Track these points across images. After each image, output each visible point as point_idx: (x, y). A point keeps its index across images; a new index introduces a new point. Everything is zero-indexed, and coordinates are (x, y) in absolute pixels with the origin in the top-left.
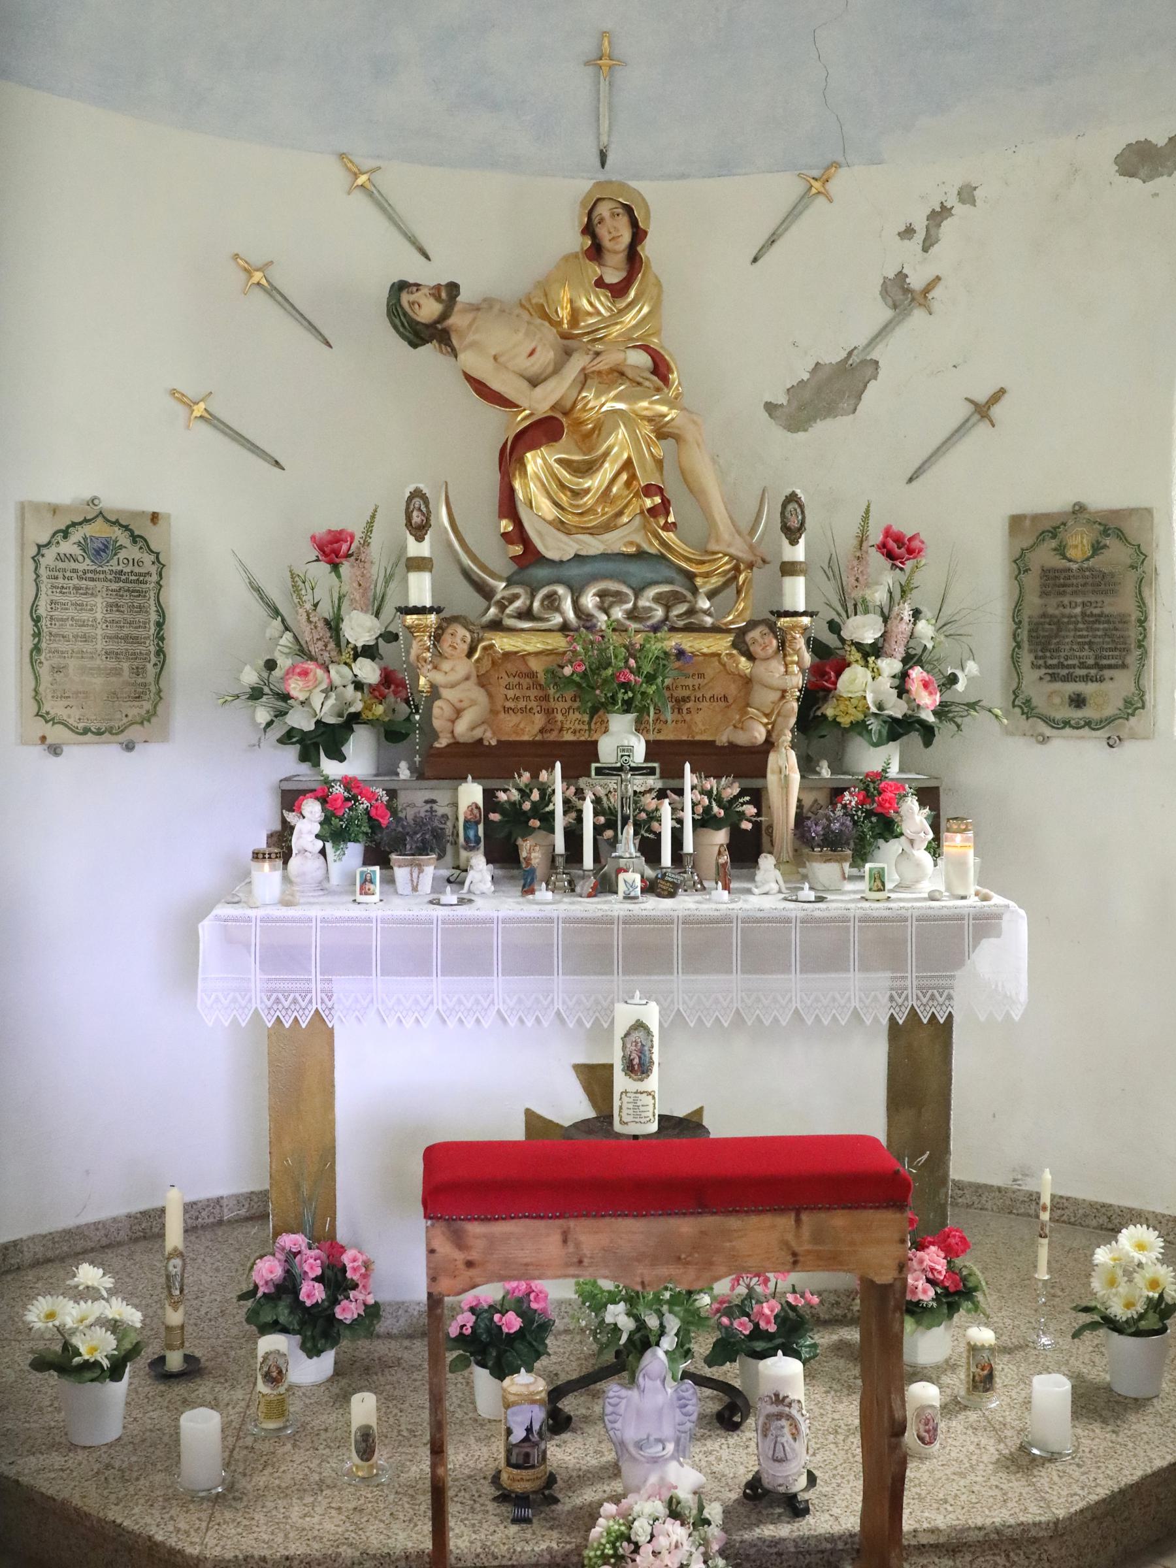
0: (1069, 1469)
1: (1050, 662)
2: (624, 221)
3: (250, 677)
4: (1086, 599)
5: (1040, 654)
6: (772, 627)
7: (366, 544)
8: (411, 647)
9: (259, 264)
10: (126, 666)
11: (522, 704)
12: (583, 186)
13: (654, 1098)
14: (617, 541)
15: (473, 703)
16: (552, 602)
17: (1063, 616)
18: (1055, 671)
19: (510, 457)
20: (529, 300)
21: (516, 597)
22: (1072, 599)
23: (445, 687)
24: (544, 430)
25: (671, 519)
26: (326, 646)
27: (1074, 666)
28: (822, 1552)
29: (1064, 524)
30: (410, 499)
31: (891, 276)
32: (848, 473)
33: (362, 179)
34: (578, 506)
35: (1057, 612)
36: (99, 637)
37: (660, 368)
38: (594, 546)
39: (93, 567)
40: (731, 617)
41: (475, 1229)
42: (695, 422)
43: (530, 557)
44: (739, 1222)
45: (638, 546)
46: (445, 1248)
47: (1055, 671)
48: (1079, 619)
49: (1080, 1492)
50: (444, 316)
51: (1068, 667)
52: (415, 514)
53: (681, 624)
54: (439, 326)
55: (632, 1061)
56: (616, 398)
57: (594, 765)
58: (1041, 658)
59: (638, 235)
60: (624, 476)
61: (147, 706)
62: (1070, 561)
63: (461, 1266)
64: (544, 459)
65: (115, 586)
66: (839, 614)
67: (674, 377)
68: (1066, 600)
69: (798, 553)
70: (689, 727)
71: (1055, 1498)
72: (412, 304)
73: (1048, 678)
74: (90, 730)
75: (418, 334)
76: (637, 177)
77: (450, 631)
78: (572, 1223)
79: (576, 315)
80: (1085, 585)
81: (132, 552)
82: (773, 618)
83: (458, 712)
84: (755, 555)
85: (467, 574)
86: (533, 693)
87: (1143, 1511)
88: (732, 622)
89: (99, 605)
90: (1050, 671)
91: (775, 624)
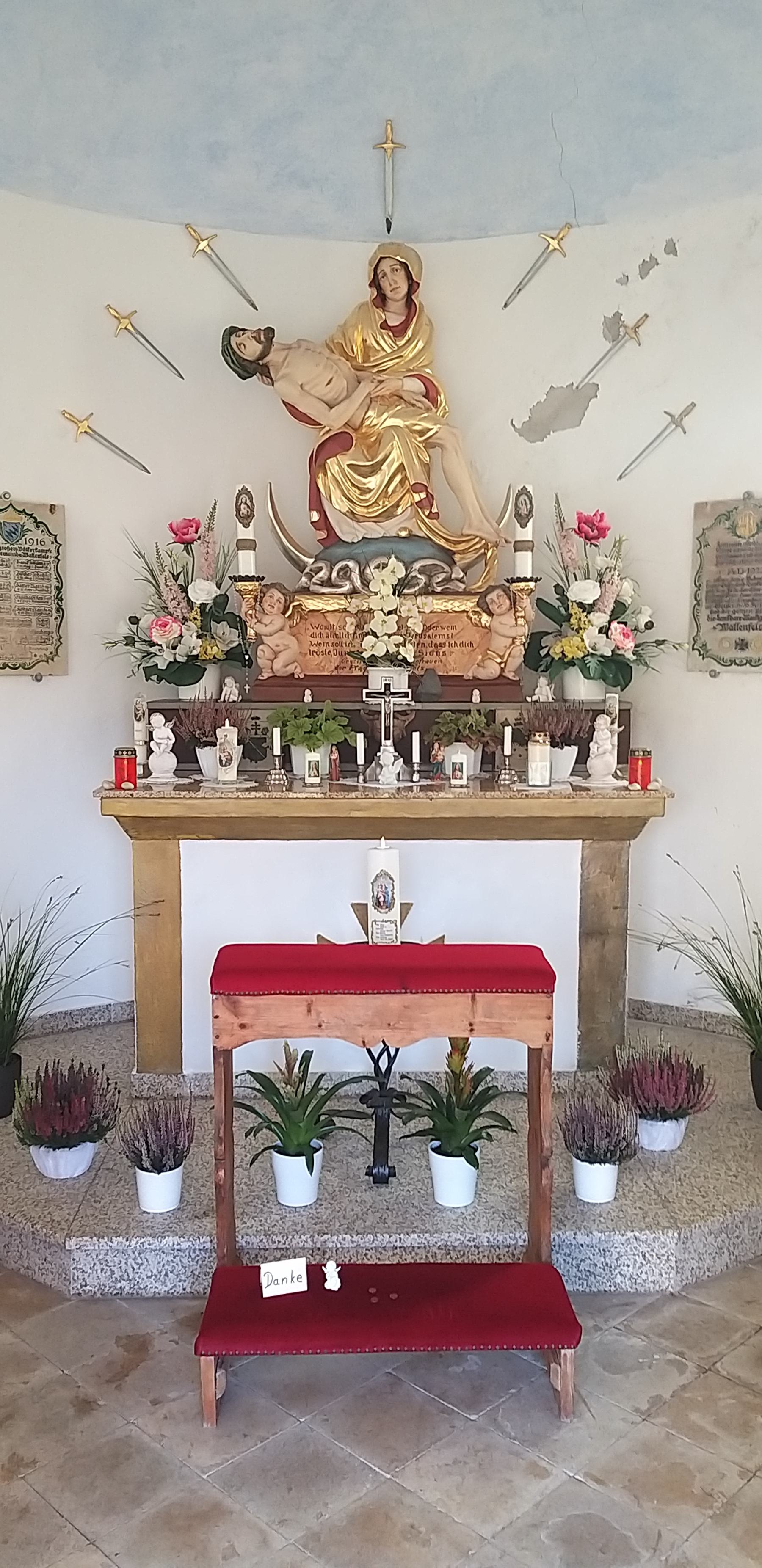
0: (696, 1199)
1: (721, 615)
2: (401, 276)
3: (124, 629)
4: (750, 567)
5: (714, 609)
6: (506, 591)
7: (210, 528)
8: (241, 607)
9: (125, 314)
10: (34, 619)
11: (322, 648)
12: (370, 249)
13: (396, 925)
14: (391, 527)
15: (287, 647)
16: (345, 573)
17: (733, 579)
18: (726, 622)
19: (317, 461)
20: (333, 342)
21: (321, 569)
22: (739, 567)
23: (266, 635)
24: (338, 442)
25: (434, 510)
26: (178, 604)
27: (740, 618)
28: (509, 1247)
29: (736, 509)
30: (238, 496)
31: (611, 316)
32: (573, 470)
33: (203, 245)
34: (367, 501)
35: (729, 577)
36: (13, 597)
37: (431, 393)
38: (376, 531)
39: (6, 546)
40: (480, 583)
41: (246, 1001)
42: (455, 435)
43: (331, 539)
44: (432, 1000)
45: (410, 531)
46: (226, 1016)
47: (726, 622)
48: (745, 582)
49: (702, 1214)
50: (264, 354)
51: (736, 619)
52: (243, 506)
53: (439, 589)
54: (261, 362)
55: (378, 899)
56: (393, 416)
57: (365, 691)
58: (715, 612)
59: (413, 286)
60: (398, 478)
61: (52, 648)
62: (740, 537)
63: (236, 1026)
64: (339, 465)
65: (24, 559)
66: (562, 580)
67: (441, 398)
68: (735, 568)
69: (526, 534)
70: (445, 665)
71: (681, 1218)
72: (238, 345)
73: (720, 627)
74: (8, 666)
75: (245, 369)
76: (417, 240)
77: (268, 594)
78: (314, 997)
79: (367, 349)
80: (751, 555)
81: (35, 534)
82: (508, 585)
83: (276, 654)
84: (499, 537)
85: (286, 551)
86: (331, 640)
87: (751, 1232)
88: (479, 588)
89: (12, 573)
90: (722, 623)
91: (509, 588)
